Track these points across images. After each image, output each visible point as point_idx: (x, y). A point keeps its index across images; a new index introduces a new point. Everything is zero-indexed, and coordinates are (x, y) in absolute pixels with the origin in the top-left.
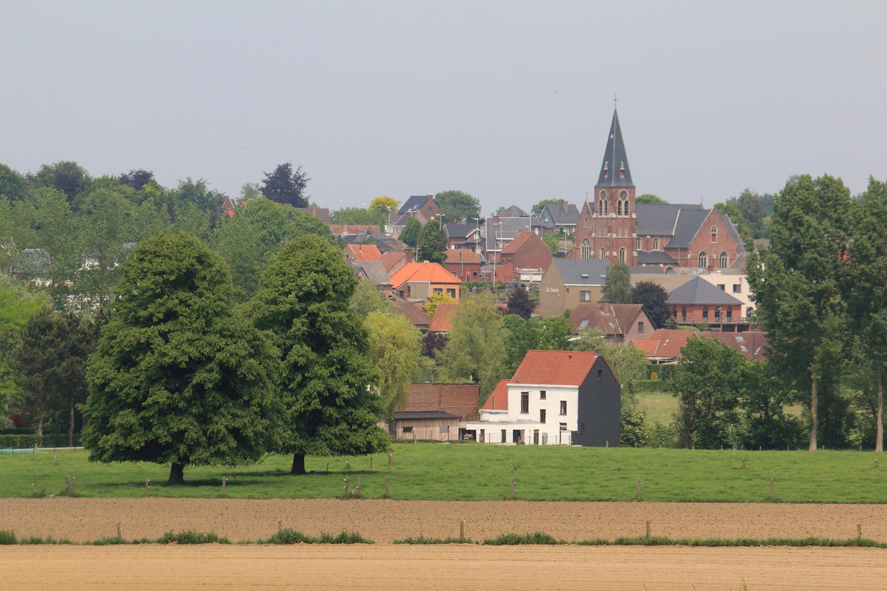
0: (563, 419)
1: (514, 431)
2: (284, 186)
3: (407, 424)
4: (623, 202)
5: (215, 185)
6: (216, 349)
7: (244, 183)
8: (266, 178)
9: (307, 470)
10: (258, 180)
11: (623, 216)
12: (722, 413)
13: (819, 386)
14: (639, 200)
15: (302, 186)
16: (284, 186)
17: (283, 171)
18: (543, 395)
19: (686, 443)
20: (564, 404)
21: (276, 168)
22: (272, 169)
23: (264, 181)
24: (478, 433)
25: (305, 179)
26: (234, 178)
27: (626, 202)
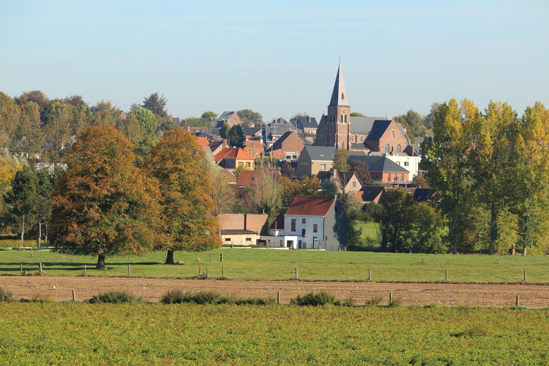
0: (315, 234)
1: (288, 241)
2: (154, 103)
3: (228, 236)
4: (344, 116)
5: (85, 99)
6: (84, 187)
7: (132, 104)
8: (145, 100)
9: (175, 261)
10: (140, 101)
11: (344, 123)
12: (404, 232)
13: (338, 202)
14: (351, 115)
15: (164, 104)
16: (154, 103)
17: (153, 98)
18: (304, 221)
19: (382, 249)
20: (315, 226)
21: (151, 95)
22: (148, 96)
23: (144, 102)
24: (267, 241)
25: (165, 101)
26: (125, 99)
27: (346, 116)
